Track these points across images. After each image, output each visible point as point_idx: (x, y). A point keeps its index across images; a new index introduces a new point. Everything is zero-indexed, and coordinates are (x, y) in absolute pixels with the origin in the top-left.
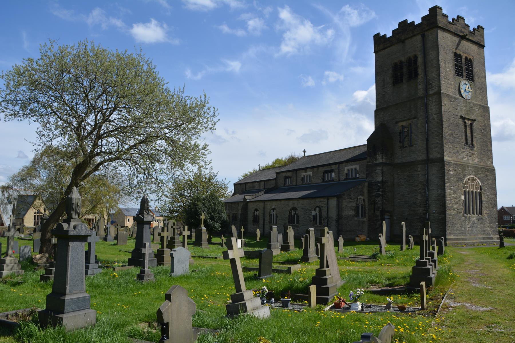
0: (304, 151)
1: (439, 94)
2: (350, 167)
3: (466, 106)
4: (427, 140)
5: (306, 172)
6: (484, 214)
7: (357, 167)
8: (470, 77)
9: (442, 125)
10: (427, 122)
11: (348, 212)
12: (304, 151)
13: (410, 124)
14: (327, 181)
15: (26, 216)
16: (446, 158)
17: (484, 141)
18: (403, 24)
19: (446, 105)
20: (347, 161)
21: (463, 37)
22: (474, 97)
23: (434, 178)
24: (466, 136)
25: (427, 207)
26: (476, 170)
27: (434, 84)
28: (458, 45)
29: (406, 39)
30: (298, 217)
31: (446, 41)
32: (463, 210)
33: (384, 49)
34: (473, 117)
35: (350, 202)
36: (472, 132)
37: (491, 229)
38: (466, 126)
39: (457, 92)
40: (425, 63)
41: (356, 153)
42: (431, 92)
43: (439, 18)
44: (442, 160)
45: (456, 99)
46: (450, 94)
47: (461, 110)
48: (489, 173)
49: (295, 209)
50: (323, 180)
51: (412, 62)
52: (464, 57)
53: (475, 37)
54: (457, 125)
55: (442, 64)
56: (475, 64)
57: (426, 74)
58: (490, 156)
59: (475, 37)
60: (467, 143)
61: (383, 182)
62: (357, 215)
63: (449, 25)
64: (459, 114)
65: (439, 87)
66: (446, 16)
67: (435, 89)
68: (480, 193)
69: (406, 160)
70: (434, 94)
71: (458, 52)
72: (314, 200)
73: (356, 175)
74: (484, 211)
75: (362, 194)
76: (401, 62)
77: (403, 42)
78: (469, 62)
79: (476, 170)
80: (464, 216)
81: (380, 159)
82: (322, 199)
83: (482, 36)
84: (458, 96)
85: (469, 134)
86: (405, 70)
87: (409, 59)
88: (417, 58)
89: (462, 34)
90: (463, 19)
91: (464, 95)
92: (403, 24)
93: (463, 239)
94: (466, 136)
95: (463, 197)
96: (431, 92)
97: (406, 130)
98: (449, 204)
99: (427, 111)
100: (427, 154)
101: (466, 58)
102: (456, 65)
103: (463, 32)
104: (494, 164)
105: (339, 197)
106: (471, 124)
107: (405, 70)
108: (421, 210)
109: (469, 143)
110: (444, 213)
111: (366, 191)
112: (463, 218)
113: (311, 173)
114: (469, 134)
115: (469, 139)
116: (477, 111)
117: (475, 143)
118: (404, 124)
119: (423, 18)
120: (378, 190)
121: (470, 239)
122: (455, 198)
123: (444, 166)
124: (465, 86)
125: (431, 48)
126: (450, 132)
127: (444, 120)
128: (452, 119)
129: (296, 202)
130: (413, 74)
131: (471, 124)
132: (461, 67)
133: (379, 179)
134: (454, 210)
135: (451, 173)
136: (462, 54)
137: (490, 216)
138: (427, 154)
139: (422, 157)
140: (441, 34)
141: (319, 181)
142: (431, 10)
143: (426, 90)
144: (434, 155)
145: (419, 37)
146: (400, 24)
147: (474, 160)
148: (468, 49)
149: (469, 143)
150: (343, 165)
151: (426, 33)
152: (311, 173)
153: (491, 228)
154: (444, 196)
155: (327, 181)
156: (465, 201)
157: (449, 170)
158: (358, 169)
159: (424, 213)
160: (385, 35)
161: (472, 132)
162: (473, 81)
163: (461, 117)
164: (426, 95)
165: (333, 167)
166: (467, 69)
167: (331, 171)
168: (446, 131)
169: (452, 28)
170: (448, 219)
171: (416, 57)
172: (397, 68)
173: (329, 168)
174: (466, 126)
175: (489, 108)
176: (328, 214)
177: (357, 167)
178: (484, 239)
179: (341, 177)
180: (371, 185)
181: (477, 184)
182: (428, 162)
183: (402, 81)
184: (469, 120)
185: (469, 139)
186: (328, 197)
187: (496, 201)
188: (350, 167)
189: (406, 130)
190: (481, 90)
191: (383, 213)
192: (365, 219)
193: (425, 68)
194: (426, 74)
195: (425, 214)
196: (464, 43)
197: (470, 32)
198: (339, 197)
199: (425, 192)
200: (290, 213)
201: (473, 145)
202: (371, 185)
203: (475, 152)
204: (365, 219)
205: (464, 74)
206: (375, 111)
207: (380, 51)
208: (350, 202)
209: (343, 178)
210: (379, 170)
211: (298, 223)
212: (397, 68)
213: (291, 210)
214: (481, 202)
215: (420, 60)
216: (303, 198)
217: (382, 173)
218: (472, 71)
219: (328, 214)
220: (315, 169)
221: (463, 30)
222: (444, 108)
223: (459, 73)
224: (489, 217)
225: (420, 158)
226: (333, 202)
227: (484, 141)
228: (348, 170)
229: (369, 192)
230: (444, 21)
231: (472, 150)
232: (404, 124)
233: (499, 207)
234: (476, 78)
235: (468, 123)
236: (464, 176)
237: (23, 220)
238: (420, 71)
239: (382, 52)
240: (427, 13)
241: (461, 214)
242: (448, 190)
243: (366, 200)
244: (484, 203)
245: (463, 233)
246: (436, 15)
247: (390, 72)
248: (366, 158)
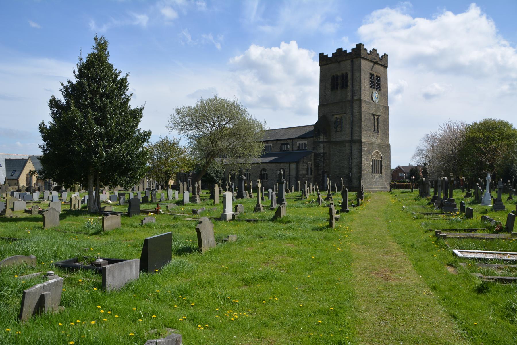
1: (360, 100)
2: (301, 142)
3: (375, 107)
4: (352, 128)
5: (267, 143)
6: (383, 173)
7: (306, 142)
8: (379, 89)
10: (352, 117)
11: (302, 172)
14: (284, 151)
15: (21, 177)
16: (363, 140)
17: (385, 129)
18: (340, 50)
19: (364, 107)
20: (298, 138)
21: (376, 63)
22: (380, 100)
23: (355, 152)
24: (375, 126)
25: (350, 169)
26: (380, 146)
27: (357, 93)
28: (372, 68)
29: (341, 61)
30: (267, 175)
31: (365, 65)
32: (371, 171)
33: (326, 65)
34: (379, 114)
36: (378, 123)
37: (386, 181)
38: (374, 120)
39: (371, 98)
40: (352, 79)
41: (304, 132)
42: (355, 98)
43: (362, 51)
44: (360, 141)
45: (369, 103)
46: (367, 100)
47: (372, 110)
48: (386, 148)
49: (264, 170)
50: (281, 150)
51: (344, 77)
52: (375, 76)
53: (381, 62)
54: (370, 120)
55: (363, 81)
56: (382, 79)
57: (352, 87)
58: (388, 138)
59: (381, 62)
60: (375, 130)
61: (324, 153)
62: (307, 174)
63: (368, 56)
64: (371, 112)
65: (361, 96)
66: (366, 50)
67: (358, 98)
68: (381, 161)
69: (339, 139)
70: (357, 100)
71: (372, 72)
72: (279, 164)
73: (305, 147)
74: (383, 172)
75: (311, 161)
76: (337, 75)
77: (339, 62)
78: (378, 77)
79: (380, 146)
81: (322, 138)
82: (285, 164)
83: (387, 61)
84: (371, 101)
85: (376, 125)
86: (339, 81)
87: (343, 75)
89: (375, 61)
90: (376, 50)
91: (374, 100)
92: (340, 50)
93: (371, 188)
94: (375, 126)
95: (371, 163)
96: (355, 98)
97: (339, 120)
98: (363, 167)
99: (352, 110)
100: (352, 137)
101: (377, 76)
102: (371, 81)
103: (375, 59)
104: (390, 143)
105: (297, 163)
106: (378, 118)
107: (339, 81)
108: (347, 171)
109: (376, 130)
110: (360, 173)
111: (313, 158)
113: (271, 145)
114: (376, 125)
115: (376, 128)
116: (382, 110)
117: (379, 130)
118: (338, 116)
119: (353, 50)
120: (321, 158)
121: (374, 188)
122: (367, 164)
123: (361, 145)
124: (376, 94)
125: (356, 70)
126: (365, 124)
127: (362, 117)
129: (265, 165)
130: (345, 85)
131: (378, 118)
132: (373, 82)
133: (322, 151)
135: (365, 148)
136: (374, 74)
137: (386, 175)
138: (352, 137)
139: (348, 138)
140: (363, 61)
141: (278, 150)
143: (353, 97)
144: (356, 138)
145: (349, 61)
146: (338, 50)
147: (377, 140)
149: (376, 130)
150: (296, 140)
151: (354, 60)
152: (271, 145)
153: (387, 181)
154: (361, 163)
155: (284, 151)
156: (372, 166)
158: (306, 143)
161: (378, 123)
162: (380, 90)
163: (372, 114)
164: (352, 100)
165: (289, 141)
166: (377, 83)
167: (287, 144)
168: (363, 124)
169: (369, 57)
170: (362, 176)
171: (347, 74)
172: (335, 79)
173: (285, 142)
174: (374, 120)
175: (388, 107)
176: (289, 173)
177: (306, 142)
178: (382, 188)
180: (316, 155)
181: (380, 155)
182: (352, 141)
183: (337, 88)
184: (376, 115)
185: (376, 128)
186: (290, 163)
187: (390, 166)
188: (301, 142)
189: (339, 120)
190: (385, 96)
191: (323, 172)
192: (312, 176)
193: (352, 83)
194: (352, 87)
195: (349, 173)
196: (376, 66)
197: (380, 59)
198: (297, 163)
200: (261, 172)
201: (378, 131)
202: (316, 155)
203: (379, 136)
204: (312, 176)
205: (375, 86)
206: (319, 106)
207: (324, 65)
209: (295, 149)
210: (321, 145)
211: (267, 179)
212: (335, 79)
213: (261, 170)
214: (381, 166)
215: (349, 77)
216: (270, 162)
217: (324, 147)
218: (379, 84)
219: (289, 173)
220: (275, 142)
223: (372, 86)
224: (385, 175)
225: (347, 139)
226: (293, 166)
227: (385, 129)
228: (300, 144)
229: (315, 159)
230: (365, 53)
231: (378, 134)
232: (338, 116)
233: (393, 166)
234: (382, 88)
235: (376, 117)
236: (373, 151)
237: (17, 180)
238: (349, 83)
239: (325, 67)
242: (363, 159)
243: (313, 164)
244: (383, 166)
245: (371, 185)
246: (361, 50)
247: (330, 81)
248: (313, 137)
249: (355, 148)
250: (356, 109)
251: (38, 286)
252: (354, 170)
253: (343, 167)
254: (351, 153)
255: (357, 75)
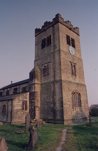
0: (12, 82)
1: (59, 50)
8: (74, 46)
9: (61, 64)
12: (12, 82)
13: (48, 65)
19: (63, 55)
23: (57, 90)
25: (55, 104)
35: (19, 102)
36: (75, 69)
40: (54, 38)
43: (60, 19)
56: (76, 41)
64: (69, 60)
72: (3, 102)
78: (73, 40)
80: (72, 108)
88: (51, 36)
98: (65, 102)
99: (54, 59)
107: (46, 42)
108: (52, 105)
110: (62, 106)
112: (72, 109)
118: (46, 65)
125: (56, 31)
127: (62, 62)
128: (65, 62)
134: (68, 105)
139: (52, 80)
142: (56, 15)
144: (57, 78)
148: (72, 35)
149: (74, 73)
154: (62, 98)
157: (64, 85)
159: (53, 107)
160: (39, 29)
161: (75, 69)
170: (64, 110)
171: (50, 36)
174: (72, 66)
179: (20, 91)
182: (54, 82)
183: (45, 47)
185: (74, 72)
199: (54, 96)
208: (19, 102)
215: (52, 37)
221: (70, 26)
222: (62, 57)
223: (68, 43)
229: (30, 97)
238: (52, 41)
240: (55, 17)
241: (71, 107)
242: (64, 95)
249: (57, 86)
250: (57, 57)
251: (64, 139)
252: (58, 105)
253: (49, 102)
254: (54, 91)
255: (56, 35)
